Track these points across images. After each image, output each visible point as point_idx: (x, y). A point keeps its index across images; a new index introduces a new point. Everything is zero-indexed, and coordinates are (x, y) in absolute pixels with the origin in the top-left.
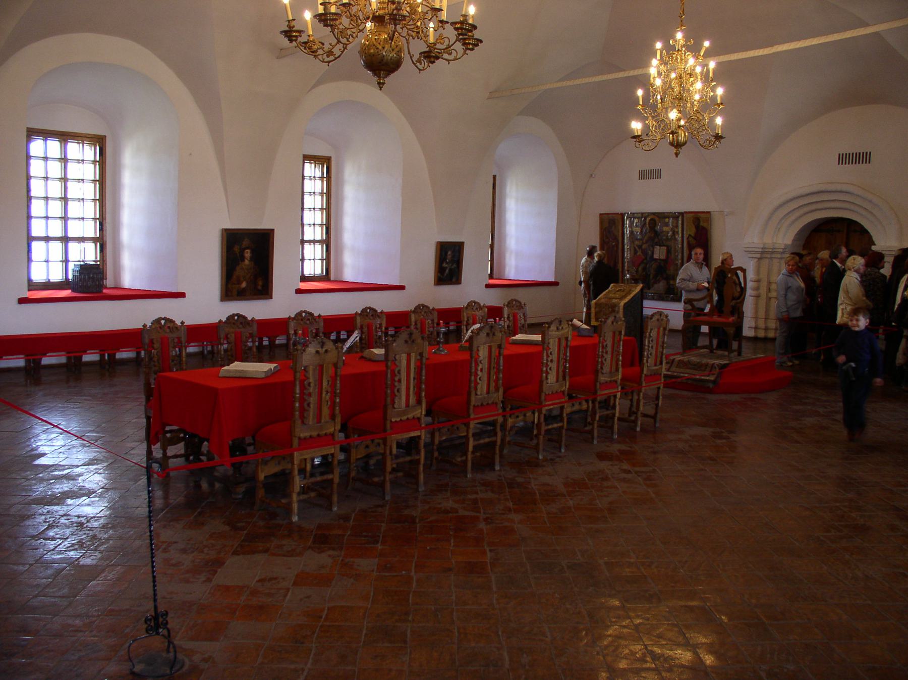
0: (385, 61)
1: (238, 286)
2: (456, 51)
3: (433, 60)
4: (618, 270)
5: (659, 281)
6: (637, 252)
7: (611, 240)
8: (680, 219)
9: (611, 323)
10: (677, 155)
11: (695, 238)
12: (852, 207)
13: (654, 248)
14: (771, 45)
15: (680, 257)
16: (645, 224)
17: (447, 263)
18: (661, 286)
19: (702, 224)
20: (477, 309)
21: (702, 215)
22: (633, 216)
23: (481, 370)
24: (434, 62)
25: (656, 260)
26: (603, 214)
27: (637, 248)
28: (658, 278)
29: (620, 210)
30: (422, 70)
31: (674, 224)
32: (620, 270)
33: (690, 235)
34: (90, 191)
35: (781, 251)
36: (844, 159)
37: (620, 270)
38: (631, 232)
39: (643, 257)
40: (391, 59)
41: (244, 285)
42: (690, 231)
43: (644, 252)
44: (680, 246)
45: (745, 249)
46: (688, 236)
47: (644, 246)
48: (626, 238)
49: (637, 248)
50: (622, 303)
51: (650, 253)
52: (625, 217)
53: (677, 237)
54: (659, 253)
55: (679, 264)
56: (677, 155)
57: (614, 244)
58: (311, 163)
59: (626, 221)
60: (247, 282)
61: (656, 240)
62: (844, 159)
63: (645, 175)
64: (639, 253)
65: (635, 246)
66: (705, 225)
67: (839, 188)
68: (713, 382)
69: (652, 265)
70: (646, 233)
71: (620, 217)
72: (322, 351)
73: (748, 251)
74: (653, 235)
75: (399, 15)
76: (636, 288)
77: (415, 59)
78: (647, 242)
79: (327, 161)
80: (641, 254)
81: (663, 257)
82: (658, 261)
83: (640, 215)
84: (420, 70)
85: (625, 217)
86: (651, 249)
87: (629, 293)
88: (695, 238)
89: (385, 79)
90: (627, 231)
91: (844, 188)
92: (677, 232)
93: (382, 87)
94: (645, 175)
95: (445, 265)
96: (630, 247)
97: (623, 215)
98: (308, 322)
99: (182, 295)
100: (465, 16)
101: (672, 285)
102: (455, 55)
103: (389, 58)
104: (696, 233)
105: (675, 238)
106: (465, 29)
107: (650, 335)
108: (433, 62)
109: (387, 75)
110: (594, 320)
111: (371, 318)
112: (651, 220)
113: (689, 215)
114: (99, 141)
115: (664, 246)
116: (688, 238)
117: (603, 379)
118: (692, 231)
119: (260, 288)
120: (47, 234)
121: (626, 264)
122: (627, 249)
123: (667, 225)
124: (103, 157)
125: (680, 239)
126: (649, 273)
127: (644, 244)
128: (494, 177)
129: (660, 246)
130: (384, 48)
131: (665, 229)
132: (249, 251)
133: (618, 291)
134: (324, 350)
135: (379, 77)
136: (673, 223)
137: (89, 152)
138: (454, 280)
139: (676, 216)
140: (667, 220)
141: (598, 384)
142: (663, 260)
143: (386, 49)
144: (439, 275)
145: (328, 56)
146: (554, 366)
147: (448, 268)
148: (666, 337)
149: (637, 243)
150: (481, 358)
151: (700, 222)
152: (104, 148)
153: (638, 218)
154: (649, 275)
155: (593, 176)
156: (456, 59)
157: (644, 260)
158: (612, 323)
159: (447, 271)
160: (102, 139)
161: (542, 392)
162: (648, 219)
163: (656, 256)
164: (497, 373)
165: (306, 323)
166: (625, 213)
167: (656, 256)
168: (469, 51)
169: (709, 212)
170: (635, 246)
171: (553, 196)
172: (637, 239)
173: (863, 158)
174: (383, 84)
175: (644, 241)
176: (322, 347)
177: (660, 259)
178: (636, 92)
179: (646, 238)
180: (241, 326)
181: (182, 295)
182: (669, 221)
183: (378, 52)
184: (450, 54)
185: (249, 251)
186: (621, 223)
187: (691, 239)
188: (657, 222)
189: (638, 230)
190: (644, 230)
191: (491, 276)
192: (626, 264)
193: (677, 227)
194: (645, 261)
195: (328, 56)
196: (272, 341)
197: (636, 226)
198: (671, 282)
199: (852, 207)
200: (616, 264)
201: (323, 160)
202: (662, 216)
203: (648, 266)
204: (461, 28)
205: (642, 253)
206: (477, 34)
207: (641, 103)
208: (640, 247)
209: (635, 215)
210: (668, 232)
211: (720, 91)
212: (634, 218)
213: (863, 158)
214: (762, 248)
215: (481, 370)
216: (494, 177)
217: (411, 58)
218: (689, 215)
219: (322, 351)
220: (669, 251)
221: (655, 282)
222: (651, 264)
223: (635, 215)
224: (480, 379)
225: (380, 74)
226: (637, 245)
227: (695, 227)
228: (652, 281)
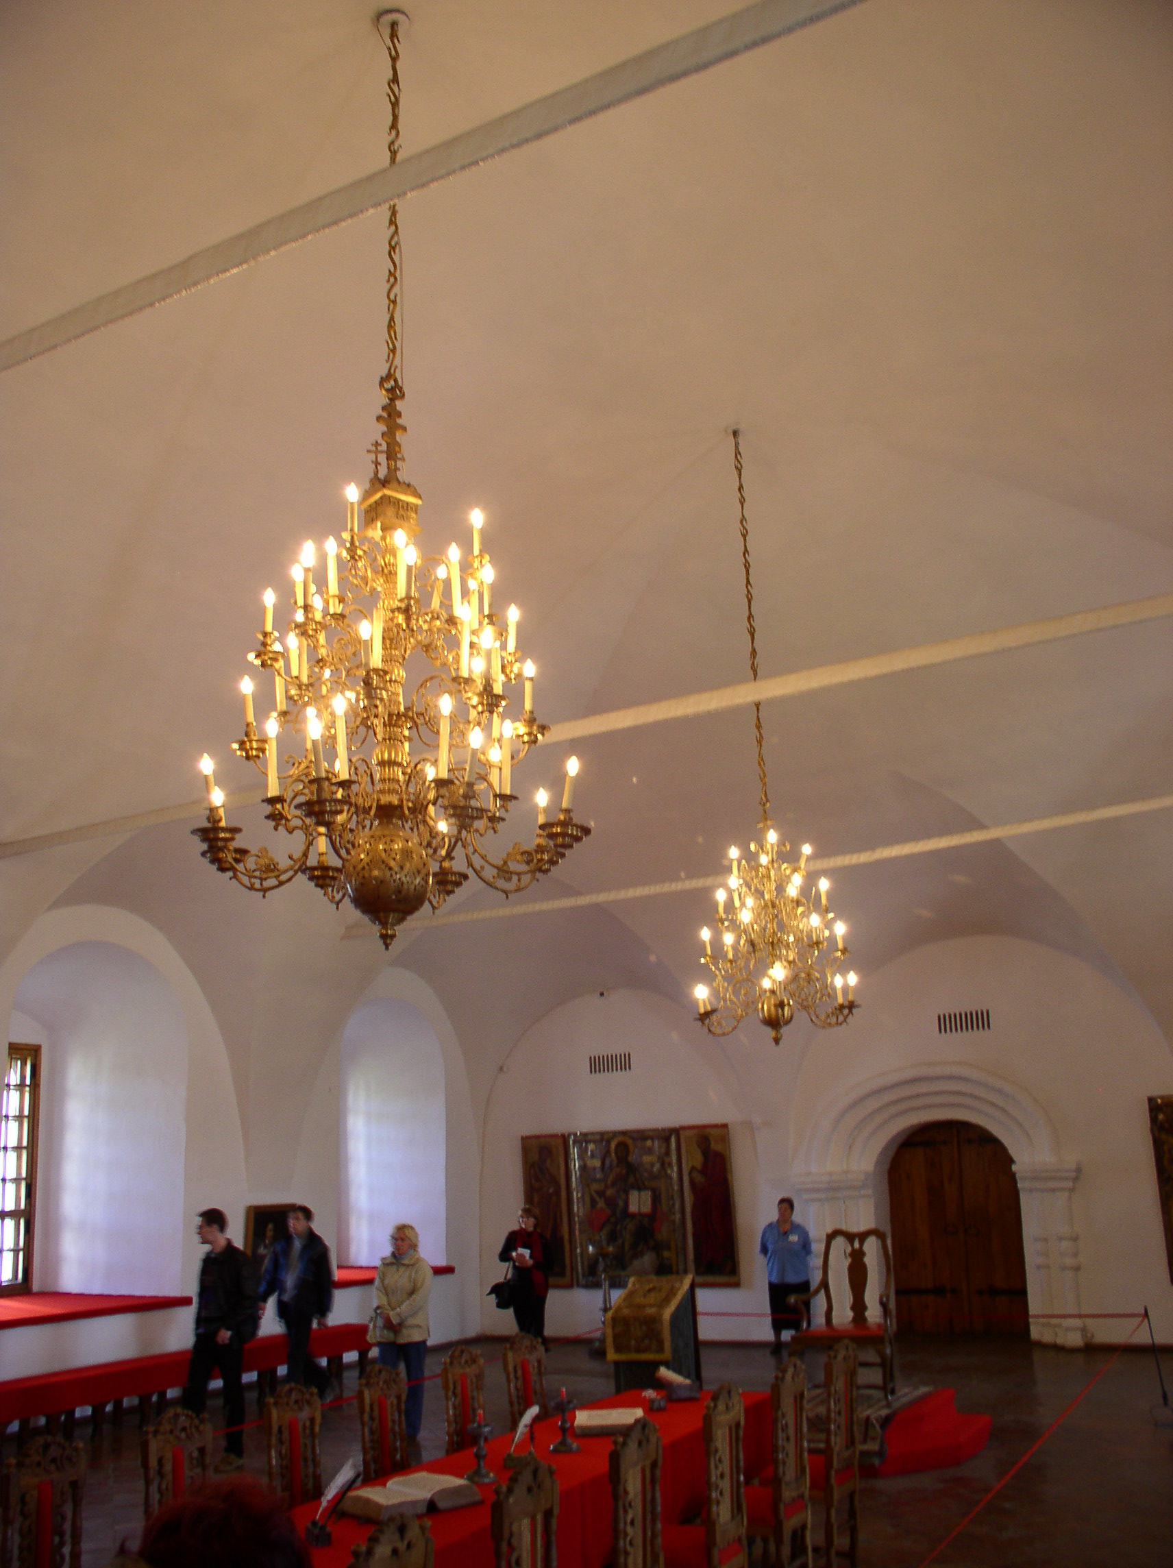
0: (404, 892)
3: (450, 888)
4: (562, 1238)
8: (673, 1139)
9: (791, 1380)
10: (777, 1041)
12: (968, 1101)
13: (627, 1195)
14: (872, 847)
15: (677, 1206)
16: (608, 1152)
20: (466, 1362)
21: (714, 1132)
23: (632, 1523)
24: (452, 892)
25: (633, 1216)
27: (595, 1195)
29: (557, 1126)
31: (663, 1150)
32: (566, 1237)
33: (693, 1169)
36: (947, 1023)
37: (566, 1237)
38: (583, 1168)
40: (415, 889)
42: (693, 1159)
43: (610, 1202)
44: (676, 1188)
47: (609, 1192)
48: (574, 1179)
49: (595, 1195)
50: (668, 1313)
51: (621, 1203)
52: (571, 1142)
53: (669, 1172)
54: (639, 1202)
55: (677, 1221)
56: (777, 1041)
59: (571, 1146)
61: (631, 1179)
62: (947, 1023)
63: (599, 1065)
64: (601, 1204)
67: (947, 1070)
68: (880, 1454)
70: (611, 1167)
71: (560, 1141)
72: (402, 1546)
75: (472, 809)
76: (682, 1282)
78: (614, 1184)
81: (647, 1208)
85: (571, 1142)
87: (672, 1293)
89: (395, 928)
90: (575, 1166)
91: (956, 1070)
92: (670, 1164)
93: (390, 944)
94: (599, 1065)
96: (583, 1196)
97: (564, 1139)
98: (183, 1435)
100: (213, 810)
103: (412, 887)
105: (666, 1173)
106: (571, 836)
107: (835, 1390)
108: (449, 893)
109: (401, 920)
110: (613, 1350)
111: (296, 1407)
112: (617, 1146)
113: (688, 1133)
115: (646, 1188)
116: (690, 1173)
117: (788, 1494)
118: (698, 1160)
121: (577, 1226)
122: (578, 1199)
123: (650, 1151)
125: (675, 1176)
129: (639, 1189)
130: (402, 868)
131: (647, 1159)
133: (650, 1290)
134: (406, 1543)
135: (384, 924)
136: (660, 1147)
139: (666, 1135)
140: (649, 1143)
141: (782, 1506)
142: (646, 1215)
143: (406, 871)
146: (725, 1485)
149: (595, 1186)
150: (631, 1496)
151: (710, 1144)
153: (594, 1142)
155: (505, 1069)
156: (518, 890)
158: (793, 1378)
161: (715, 1544)
162: (613, 1145)
163: (633, 1208)
164: (653, 1521)
165: (178, 1438)
166: (569, 1135)
167: (633, 1208)
169: (725, 1126)
171: (436, 1108)
172: (595, 1180)
173: (977, 1020)
174: (393, 936)
175: (609, 1182)
176: (402, 1537)
177: (640, 1214)
179: (611, 1178)
180: (53, 1467)
182: (653, 1144)
183: (391, 876)
186: (561, 1149)
187: (695, 1174)
188: (631, 1148)
189: (597, 1163)
190: (607, 1162)
192: (577, 1226)
193: (668, 1153)
197: (593, 1156)
199: (968, 1101)
200: (556, 1228)
202: (641, 1136)
203: (619, 1227)
204: (564, 835)
206: (239, 842)
207: (709, 952)
208: (601, 1193)
209: (589, 1137)
210: (652, 1165)
211: (840, 929)
212: (587, 1142)
213: (977, 1020)
215: (632, 1523)
218: (688, 1133)
219: (402, 1546)
220: (656, 1200)
223: (589, 1137)
224: (631, 1543)
225: (387, 918)
227: (702, 1152)
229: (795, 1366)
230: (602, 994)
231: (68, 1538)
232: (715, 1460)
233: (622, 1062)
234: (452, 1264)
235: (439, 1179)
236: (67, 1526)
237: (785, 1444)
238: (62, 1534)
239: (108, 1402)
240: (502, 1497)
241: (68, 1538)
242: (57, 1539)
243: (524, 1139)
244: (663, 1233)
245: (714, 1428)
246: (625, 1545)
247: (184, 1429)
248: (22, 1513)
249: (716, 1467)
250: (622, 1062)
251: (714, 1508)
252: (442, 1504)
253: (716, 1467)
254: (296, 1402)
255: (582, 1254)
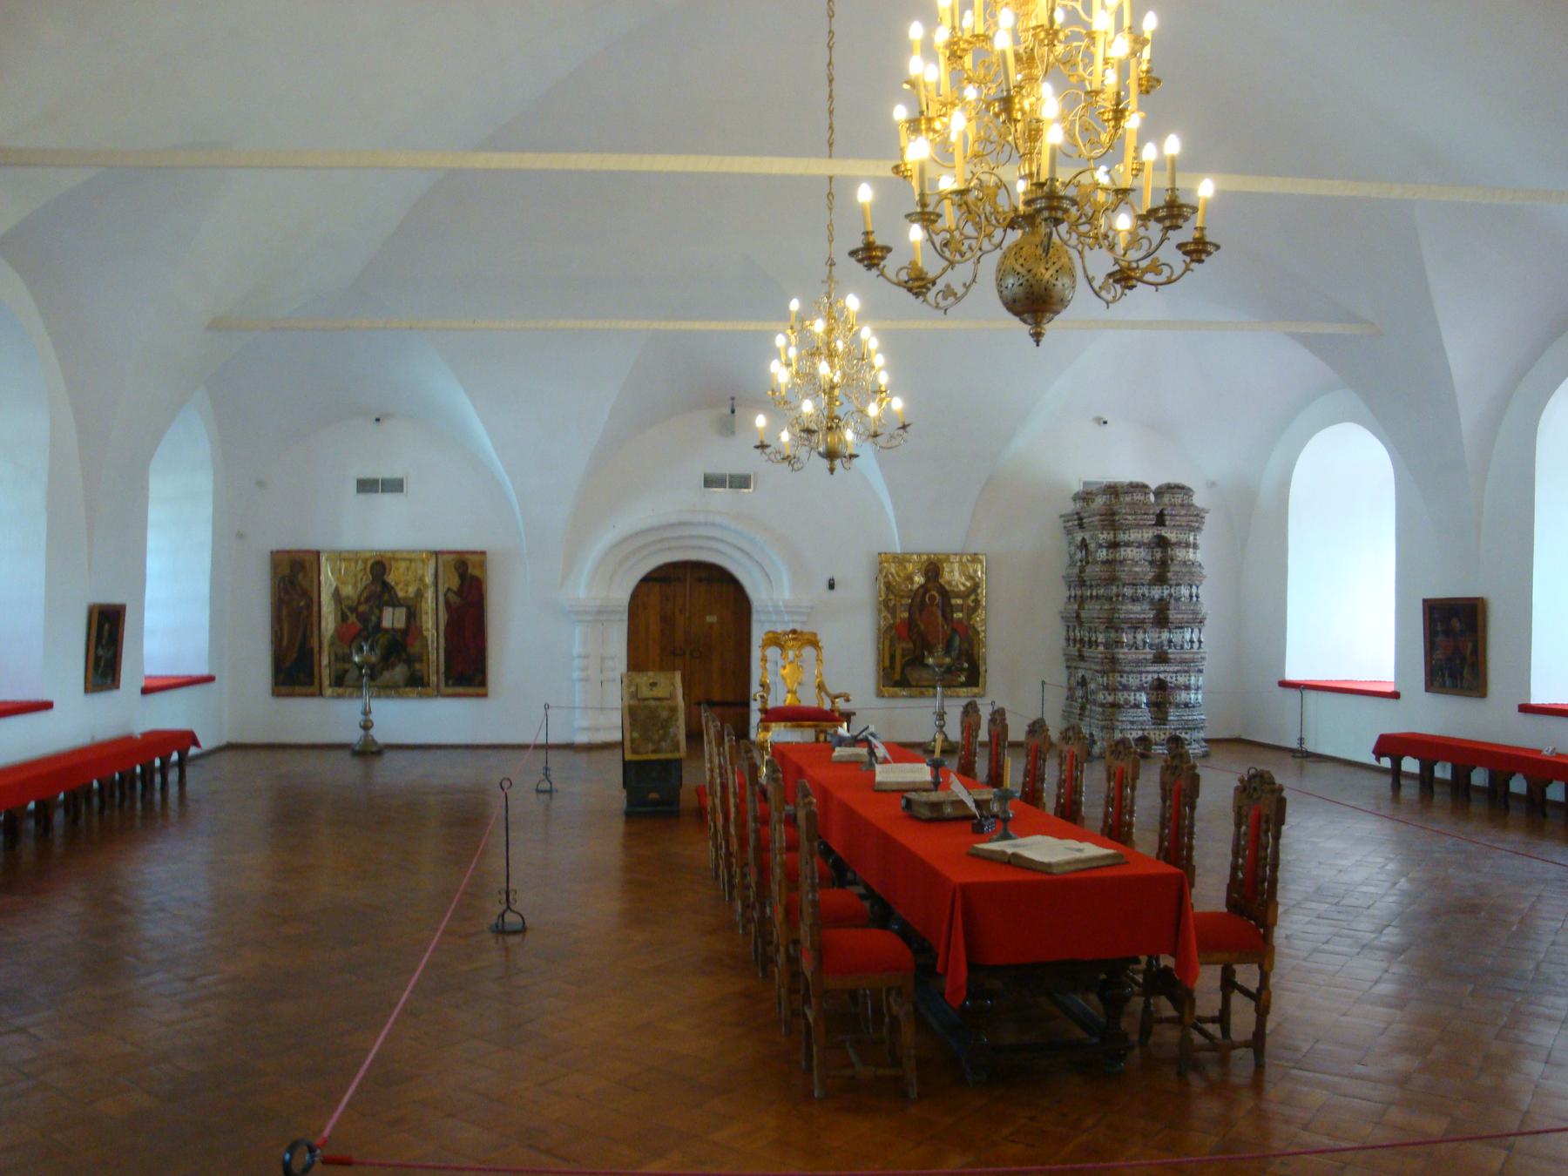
2: (1170, 267)
4: (312, 649)
18: (399, 672)
22: (340, 556)
25: (386, 630)
30: (1111, 302)
33: (449, 589)
43: (363, 618)
57: (302, 604)
61: (386, 597)
64: (352, 618)
66: (476, 572)
69: (378, 640)
77: (1096, 284)
80: (355, 620)
84: (1108, 303)
86: (377, 612)
99: (47, 706)
102: (1169, 274)
113: (447, 557)
116: (445, 595)
118: (455, 583)
145: (945, 298)
156: (1169, 282)
167: (386, 623)
168: (1197, 264)
177: (393, 629)
178: (768, 367)
181: (47, 706)
184: (1159, 273)
187: (450, 595)
195: (945, 298)
198: (418, 666)
205: (357, 617)
217: (1090, 283)
218: (447, 557)
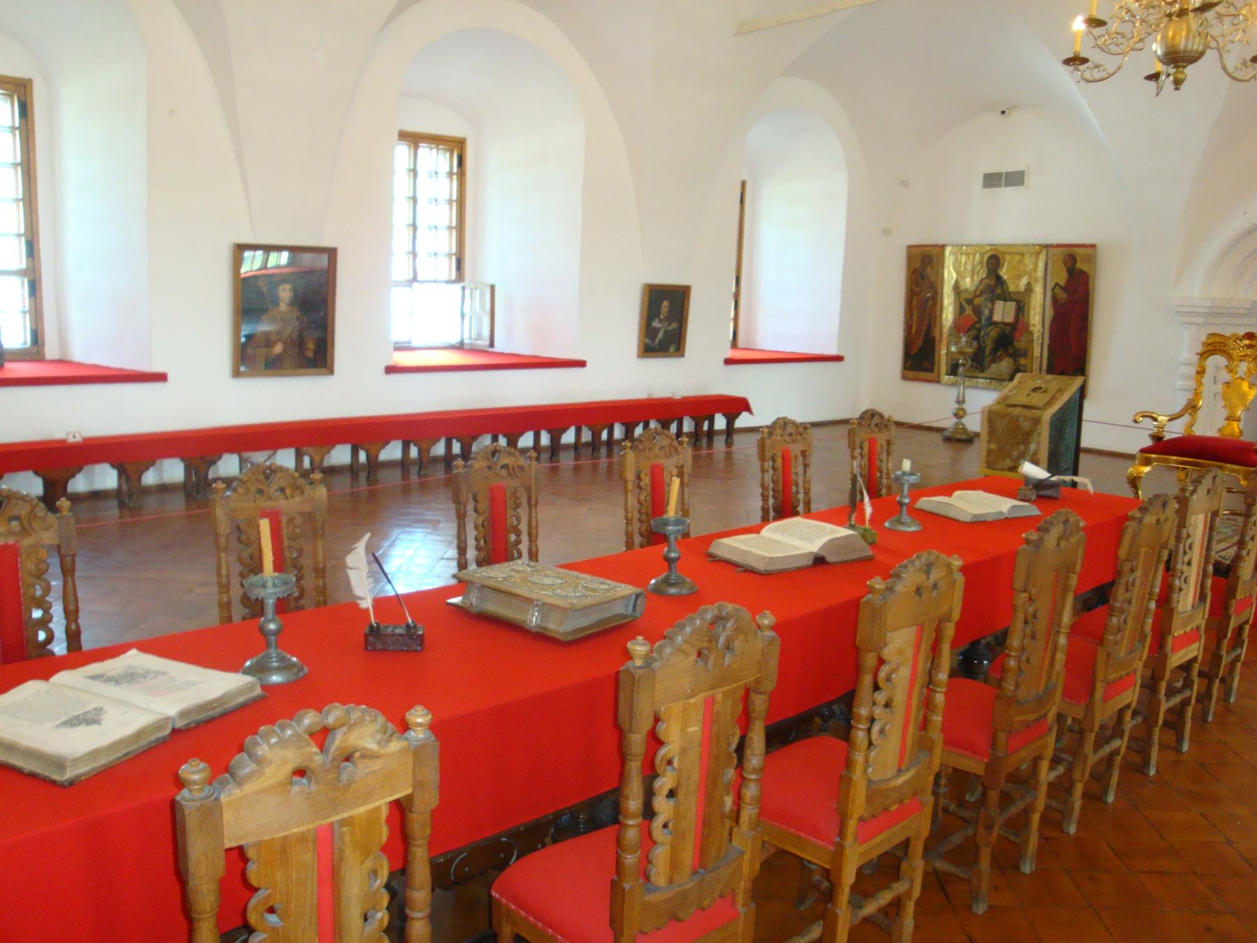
1: (266, 350)
5: (1000, 359)
6: (965, 310)
7: (924, 288)
11: (1064, 289)
13: (993, 304)
17: (660, 321)
19: (1079, 265)
25: (996, 324)
26: (912, 246)
28: (999, 353)
33: (1057, 284)
34: (446, 215)
35: (1245, 312)
39: (975, 319)
41: (278, 349)
43: (977, 311)
45: (1178, 309)
46: (1053, 285)
47: (977, 301)
51: (986, 312)
54: (1003, 312)
57: (929, 295)
58: (431, 149)
60: (285, 343)
61: (999, 291)
63: (992, 180)
64: (969, 311)
65: (962, 300)
73: (1181, 312)
74: (992, 283)
79: (459, 145)
81: (1009, 319)
82: (1000, 325)
83: (970, 250)
86: (989, 305)
88: (1064, 289)
94: (992, 180)
95: (656, 324)
101: (1023, 365)
104: (1068, 282)
114: (457, 146)
116: (1053, 290)
119: (310, 354)
120: (1005, 304)
124: (27, 120)
126: (983, 345)
127: (978, 296)
128: (743, 184)
129: (1005, 300)
132: (288, 287)
137: (435, 161)
138: (672, 349)
144: (647, 340)
147: (663, 330)
148: (630, 495)
151: (1076, 262)
152: (28, 103)
154: (985, 347)
157: (976, 323)
159: (661, 335)
160: (25, 87)
163: (997, 317)
167: (997, 317)
169: (1093, 246)
170: (962, 300)
177: (1003, 323)
185: (288, 287)
187: (1058, 290)
191: (734, 344)
194: (978, 326)
196: (555, 439)
201: (453, 144)
203: (982, 333)
208: (969, 302)
214: (1210, 307)
216: (743, 184)
221: (994, 361)
222: (988, 330)
226: (965, 299)
228: (988, 359)
229: (1066, 522)
230: (1003, 112)
231: (525, 538)
232: (1184, 546)
233: (1015, 179)
234: (841, 354)
235: (835, 276)
236: (523, 527)
237: (1185, 568)
238: (518, 534)
239: (637, 425)
240: (1187, 494)
241: (525, 538)
242: (513, 537)
243: (910, 248)
244: (1020, 344)
245: (1189, 514)
246: (1180, 584)
247: (791, 435)
248: (476, 511)
249: (1185, 553)
250: (1015, 179)
251: (1175, 596)
252: (830, 559)
253: (1185, 553)
254: (877, 425)
255: (947, 353)
